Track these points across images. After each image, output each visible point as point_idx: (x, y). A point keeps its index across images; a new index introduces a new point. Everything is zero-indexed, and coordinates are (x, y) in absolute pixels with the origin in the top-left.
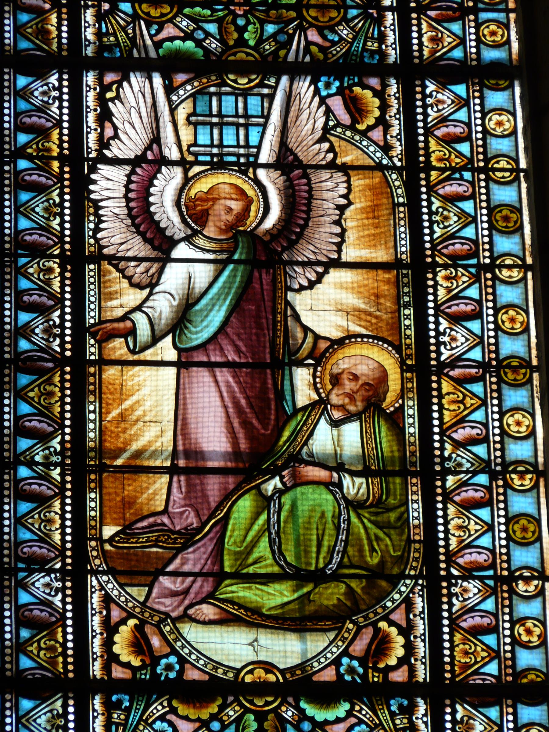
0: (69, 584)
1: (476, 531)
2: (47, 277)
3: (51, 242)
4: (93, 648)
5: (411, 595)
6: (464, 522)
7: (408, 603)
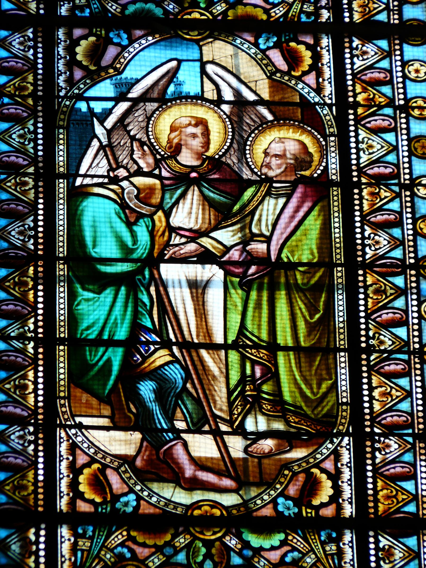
0: (41, 436)
1: (397, 397)
2: (23, 189)
3: (27, 363)
4: (60, 487)
5: (339, 448)
6: (369, 95)
7: (336, 454)
